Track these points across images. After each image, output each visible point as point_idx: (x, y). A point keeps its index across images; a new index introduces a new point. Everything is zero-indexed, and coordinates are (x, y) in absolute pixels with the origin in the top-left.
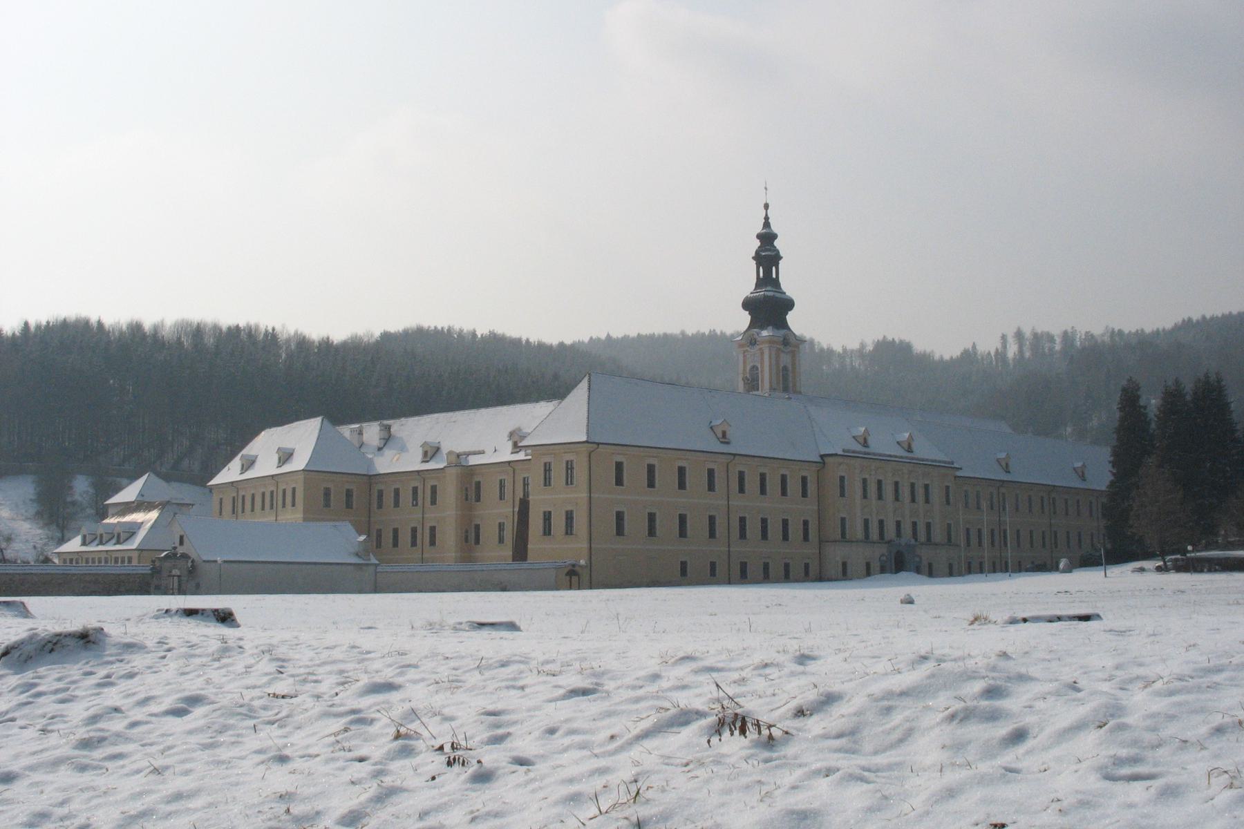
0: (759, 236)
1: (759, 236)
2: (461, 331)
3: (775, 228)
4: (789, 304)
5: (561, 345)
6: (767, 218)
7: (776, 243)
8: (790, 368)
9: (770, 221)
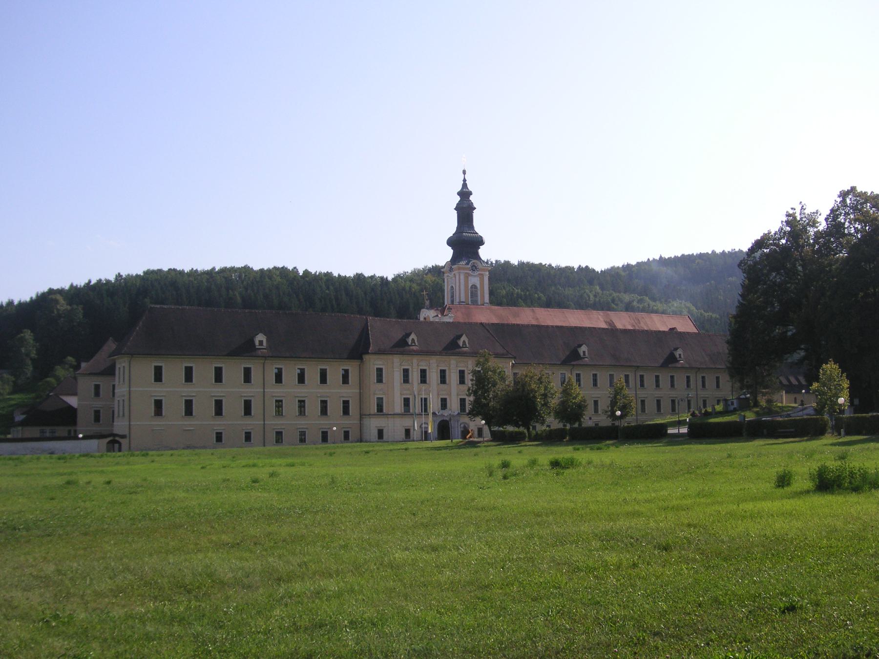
3: (470, 187)
6: (465, 180)
8: (478, 286)
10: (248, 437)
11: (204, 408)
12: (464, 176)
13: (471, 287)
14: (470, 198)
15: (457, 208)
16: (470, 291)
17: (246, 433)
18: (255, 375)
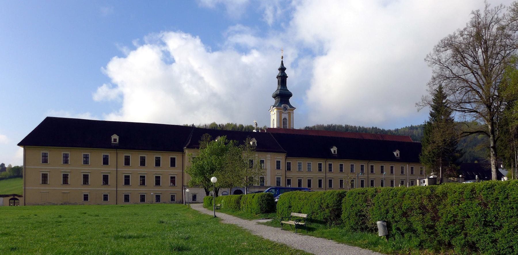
0: (279, 69)
2: (360, 127)
3: (285, 66)
4: (290, 95)
6: (282, 62)
8: (288, 119)
10: (106, 198)
11: (75, 180)
13: (284, 119)
14: (285, 72)
16: (282, 121)
17: (84, 195)
18: (112, 160)
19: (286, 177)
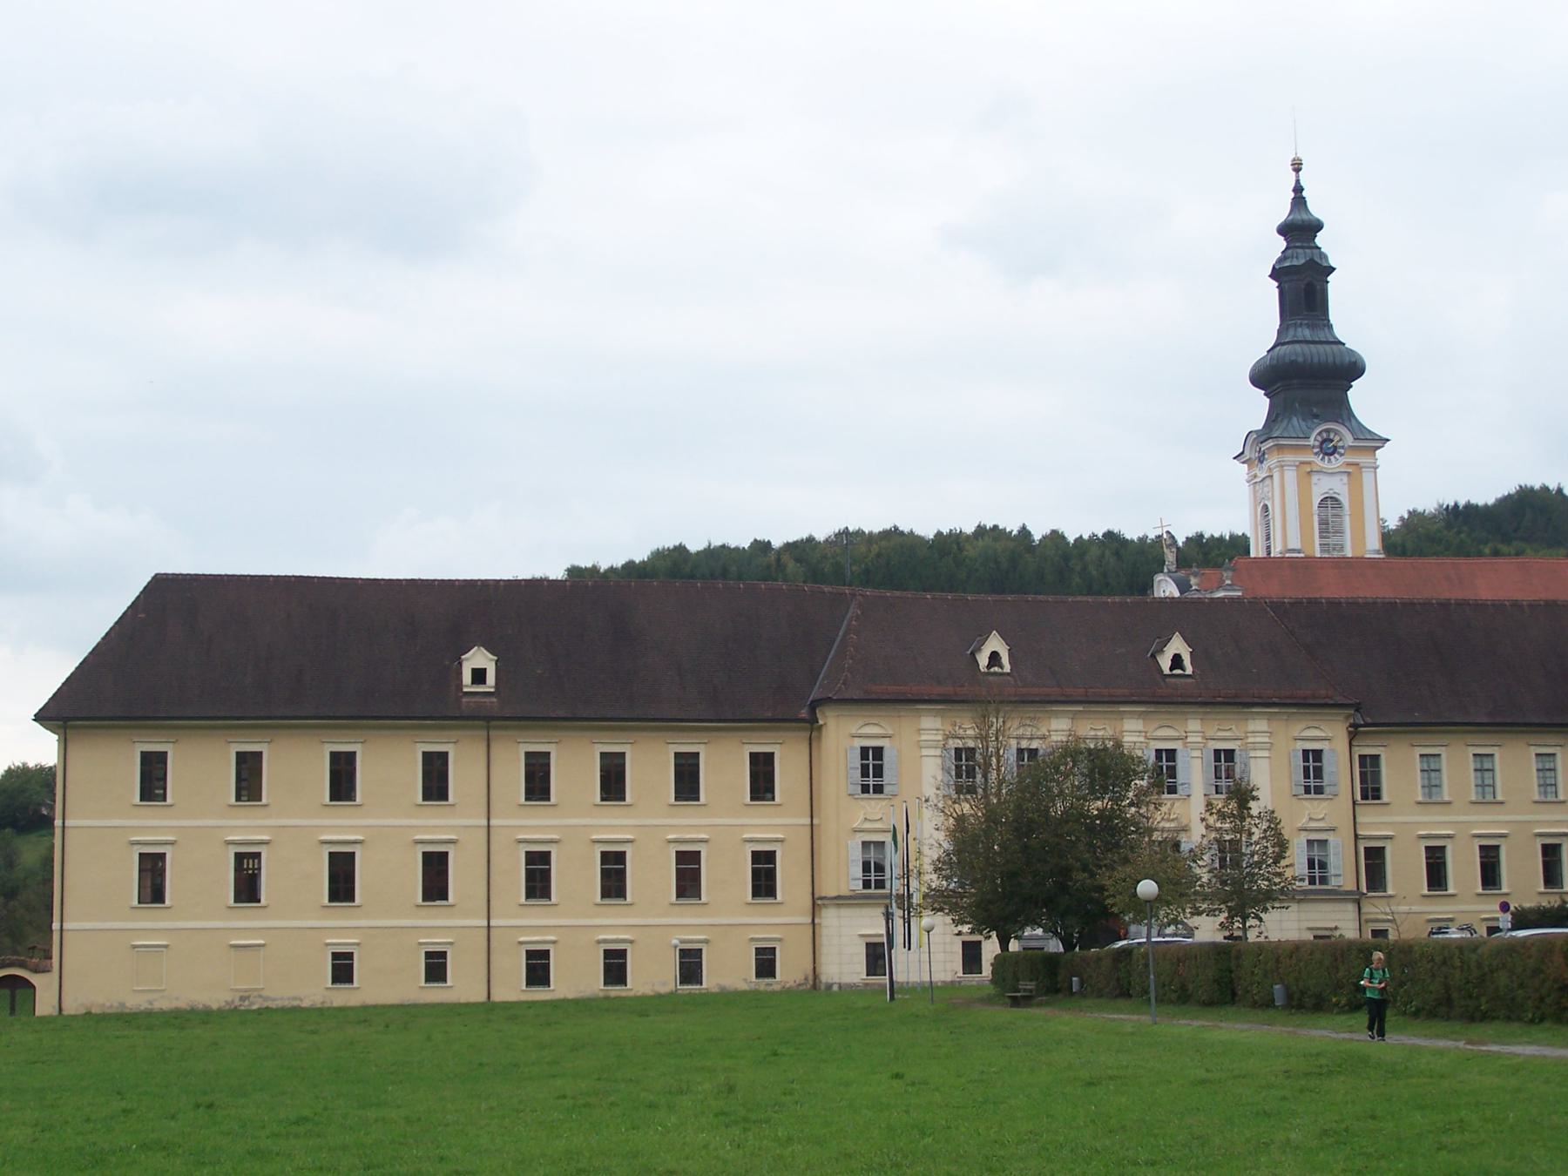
1: (1284, 230)
3: (1316, 209)
5: (1056, 537)
6: (1298, 189)
7: (1321, 239)
8: (1344, 499)
9: (1304, 194)
12: (1298, 177)
14: (1317, 240)
15: (1278, 274)
18: (463, 774)
19: (1356, 836)
